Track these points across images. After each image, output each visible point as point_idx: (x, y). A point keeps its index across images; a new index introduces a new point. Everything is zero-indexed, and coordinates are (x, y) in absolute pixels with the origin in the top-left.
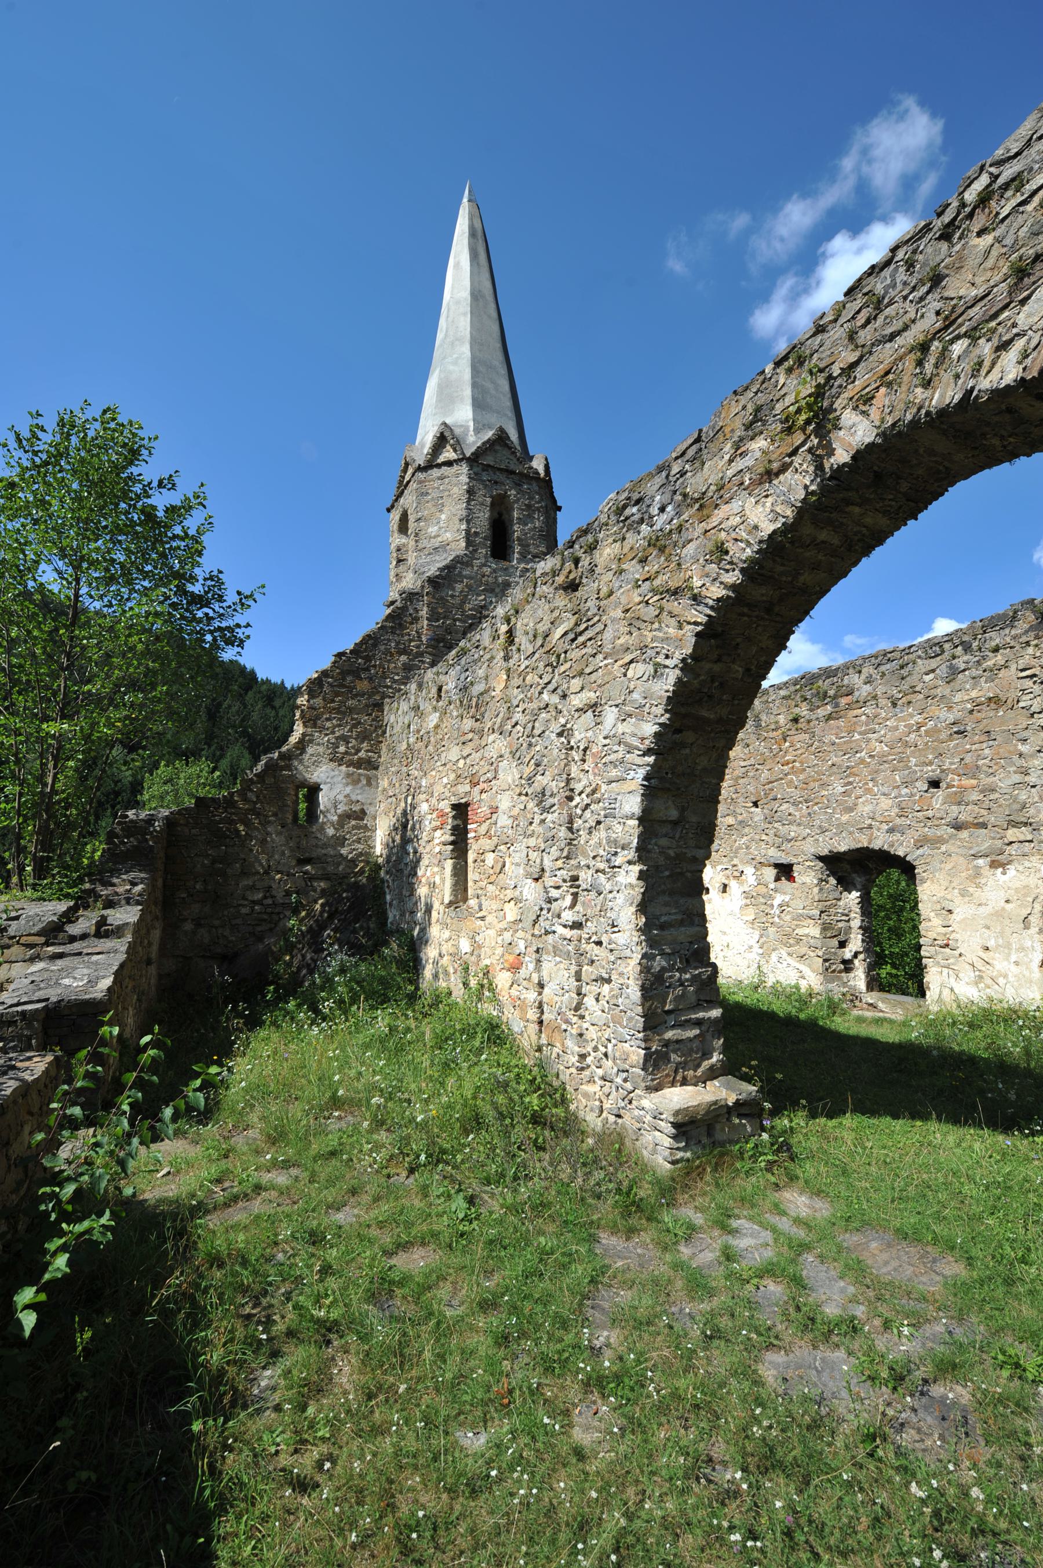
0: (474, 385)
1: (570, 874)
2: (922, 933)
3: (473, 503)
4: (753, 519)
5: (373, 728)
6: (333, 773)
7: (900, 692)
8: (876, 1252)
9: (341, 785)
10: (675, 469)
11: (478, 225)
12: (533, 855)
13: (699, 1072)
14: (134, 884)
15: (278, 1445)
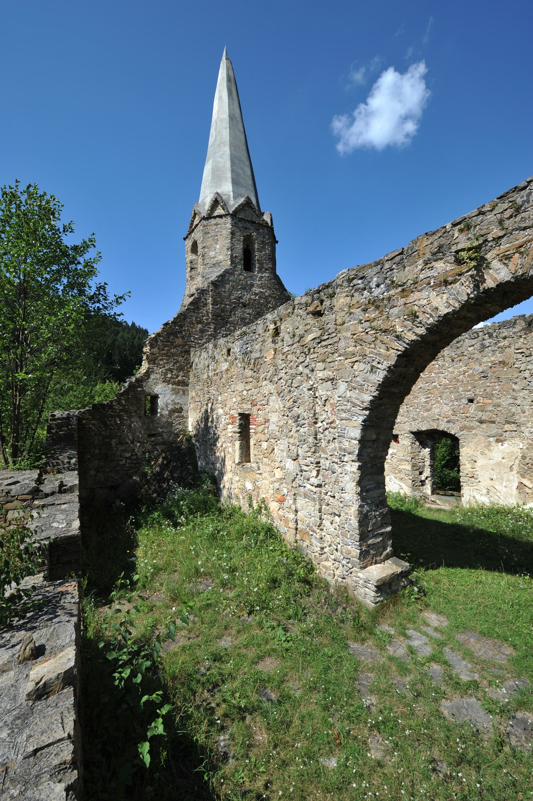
0: (233, 171)
1: (316, 461)
2: (461, 470)
3: (234, 240)
4: (435, 304)
5: (185, 364)
6: (165, 389)
7: (456, 354)
8: (474, 644)
9: (169, 395)
10: (387, 266)
11: (231, 74)
12: (292, 448)
13: (382, 557)
14: (70, 458)
15: (243, 778)
